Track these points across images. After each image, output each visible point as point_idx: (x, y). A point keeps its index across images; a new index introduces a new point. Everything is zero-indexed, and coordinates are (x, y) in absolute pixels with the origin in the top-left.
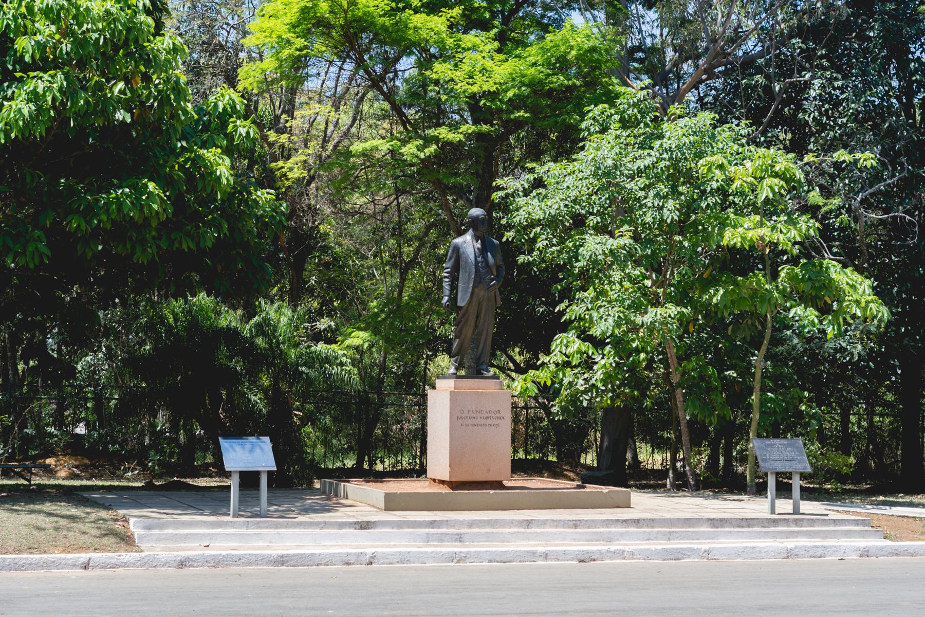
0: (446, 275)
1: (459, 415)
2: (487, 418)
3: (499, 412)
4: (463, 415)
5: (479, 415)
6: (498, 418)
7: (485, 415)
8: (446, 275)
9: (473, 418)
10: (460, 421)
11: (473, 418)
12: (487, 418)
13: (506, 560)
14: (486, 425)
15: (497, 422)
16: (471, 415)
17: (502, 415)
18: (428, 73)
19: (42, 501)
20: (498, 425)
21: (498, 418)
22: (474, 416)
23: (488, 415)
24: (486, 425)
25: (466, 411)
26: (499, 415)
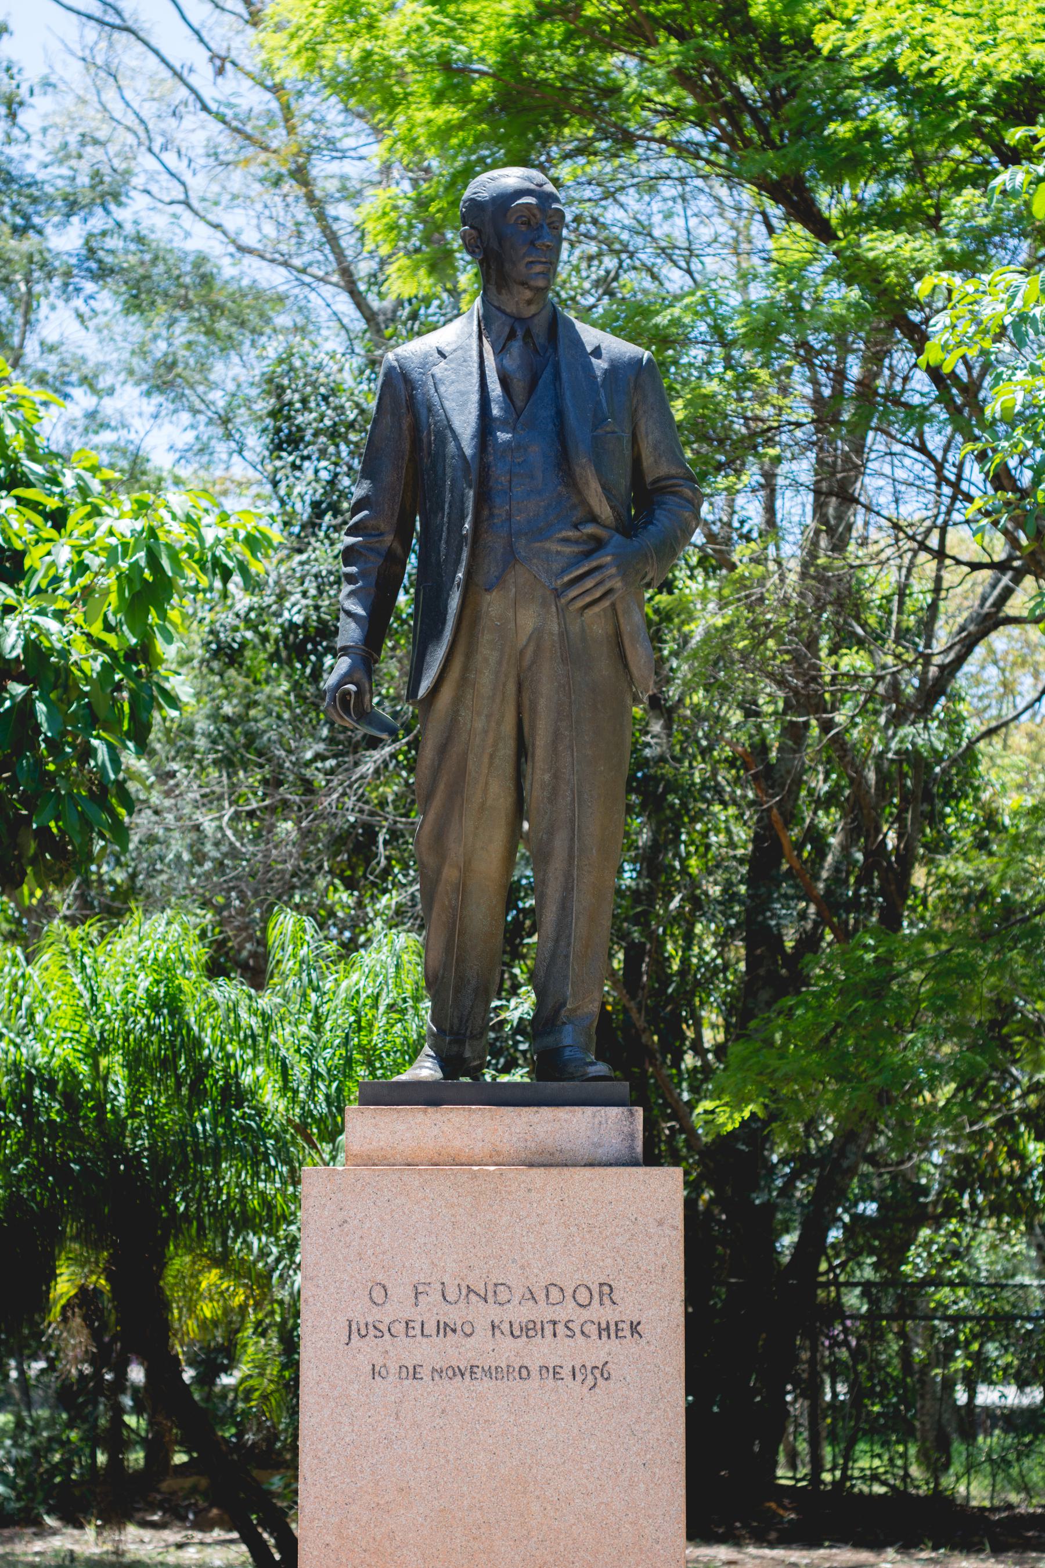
0: (966, 1197)
1: (361, 1312)
2: (529, 1330)
3: (607, 1291)
4: (385, 1316)
5: (482, 1314)
6: (604, 1330)
7: (521, 1313)
8: (966, 1197)
9: (445, 1328)
10: (368, 1351)
11: (445, 1328)
12: (529, 1330)
13: (207, 39)
14: (523, 1372)
15: (595, 1352)
16: (432, 1309)
17: (627, 1311)
18: (379, 923)
19: (421, 440)
20: (602, 1372)
21: (604, 1330)
22: (453, 1315)
23: (543, 1312)
24: (523, 1372)
25: (401, 1292)
26: (606, 1314)
